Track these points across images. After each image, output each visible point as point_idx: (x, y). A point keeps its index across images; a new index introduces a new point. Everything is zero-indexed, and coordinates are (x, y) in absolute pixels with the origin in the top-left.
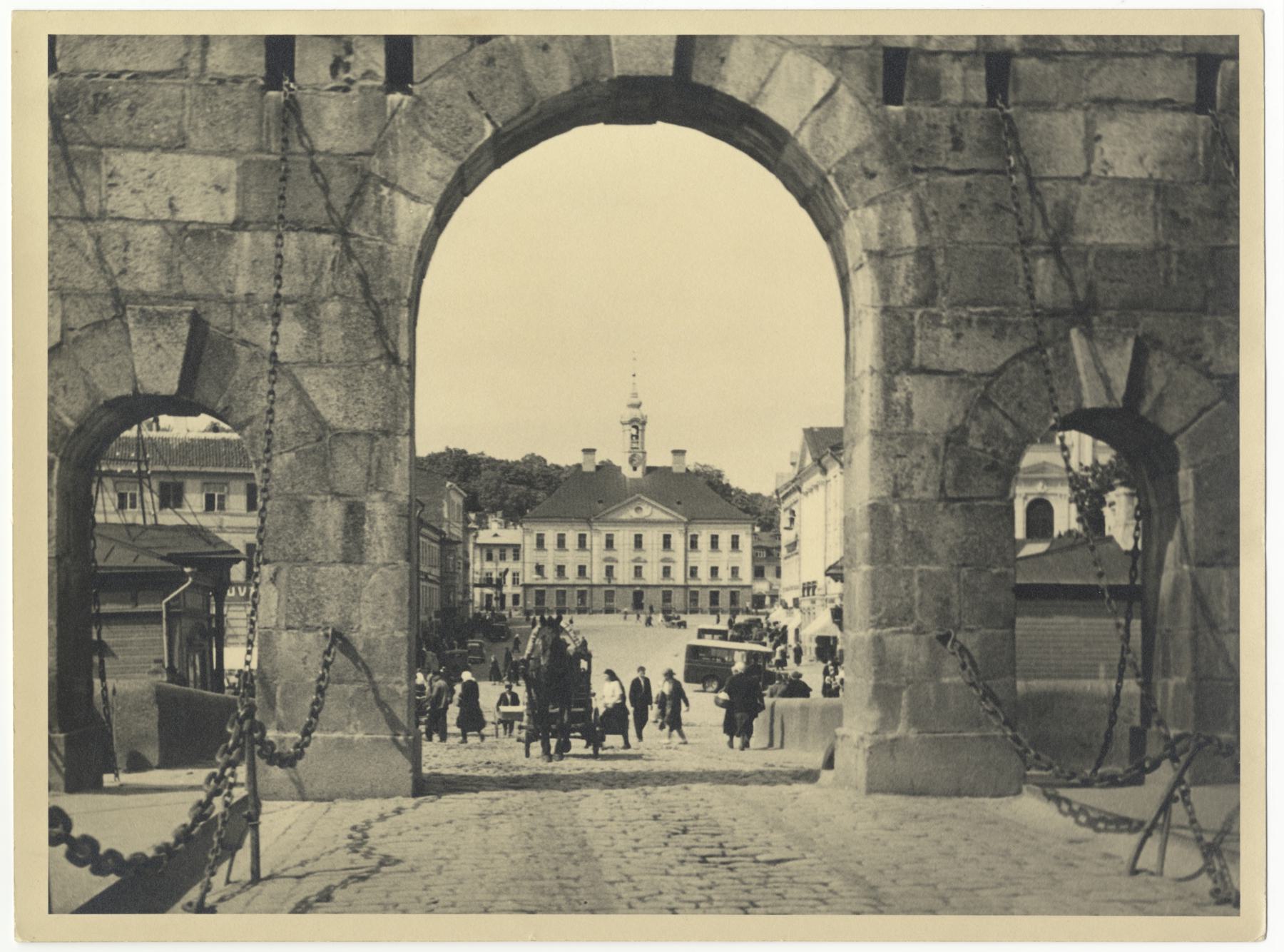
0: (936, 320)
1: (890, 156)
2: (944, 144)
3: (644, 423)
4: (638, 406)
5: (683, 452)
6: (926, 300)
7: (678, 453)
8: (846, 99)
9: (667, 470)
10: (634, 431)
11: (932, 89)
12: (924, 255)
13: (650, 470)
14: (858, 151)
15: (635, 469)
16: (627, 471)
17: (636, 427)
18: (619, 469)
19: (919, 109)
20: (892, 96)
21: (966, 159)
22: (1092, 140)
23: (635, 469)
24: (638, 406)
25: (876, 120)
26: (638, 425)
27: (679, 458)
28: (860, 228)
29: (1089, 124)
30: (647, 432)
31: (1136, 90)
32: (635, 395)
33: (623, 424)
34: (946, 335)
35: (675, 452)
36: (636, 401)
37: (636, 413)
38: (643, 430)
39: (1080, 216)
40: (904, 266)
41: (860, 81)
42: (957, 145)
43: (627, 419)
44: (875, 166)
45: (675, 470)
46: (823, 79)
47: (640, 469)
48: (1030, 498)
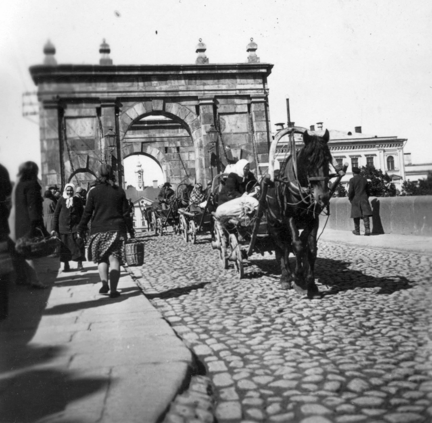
0: (173, 178)
1: (166, 159)
2: (172, 158)
3: (143, 172)
4: (140, 166)
5: (156, 181)
6: (172, 175)
7: (155, 181)
8: (161, 154)
9: (151, 188)
10: (139, 175)
11: (171, 152)
12: (171, 171)
13: (145, 188)
14: (163, 159)
15: (140, 188)
16: (138, 189)
17: (140, 174)
18: (135, 188)
19: (169, 154)
20: (166, 152)
21: (175, 159)
22: (189, 156)
23: (140, 188)
24: (140, 166)
25: (165, 155)
26: (140, 172)
27: (155, 183)
28: (164, 167)
29: (189, 154)
30: (144, 175)
31: (255, 91)
32: (139, 162)
33: (136, 172)
34: (174, 179)
35: (154, 181)
36: (140, 165)
37: (139, 169)
38: (142, 174)
39: (188, 165)
40: (169, 172)
41: (162, 151)
42: (174, 157)
43: (137, 171)
44: (165, 160)
45: (154, 187)
46: (158, 151)
47: (142, 188)
48: (388, 156)
